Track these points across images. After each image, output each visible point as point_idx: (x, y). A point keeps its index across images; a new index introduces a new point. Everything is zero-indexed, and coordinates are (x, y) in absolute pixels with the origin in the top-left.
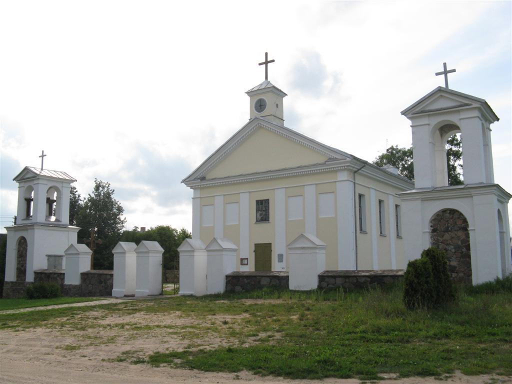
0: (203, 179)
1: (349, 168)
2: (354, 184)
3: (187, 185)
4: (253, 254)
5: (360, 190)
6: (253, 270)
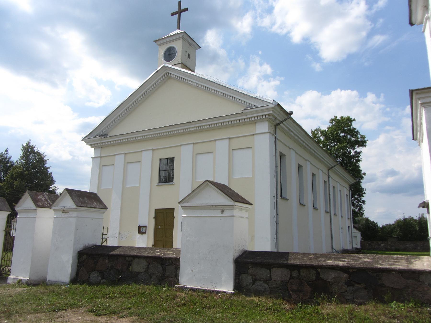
0: (105, 136)
1: (272, 117)
2: (276, 139)
3: (88, 143)
4: (153, 221)
5: (281, 148)
6: (150, 244)
